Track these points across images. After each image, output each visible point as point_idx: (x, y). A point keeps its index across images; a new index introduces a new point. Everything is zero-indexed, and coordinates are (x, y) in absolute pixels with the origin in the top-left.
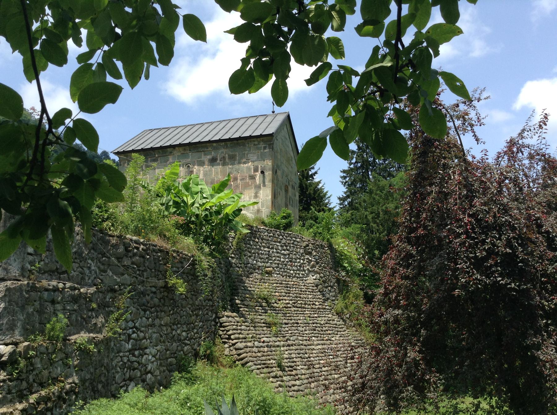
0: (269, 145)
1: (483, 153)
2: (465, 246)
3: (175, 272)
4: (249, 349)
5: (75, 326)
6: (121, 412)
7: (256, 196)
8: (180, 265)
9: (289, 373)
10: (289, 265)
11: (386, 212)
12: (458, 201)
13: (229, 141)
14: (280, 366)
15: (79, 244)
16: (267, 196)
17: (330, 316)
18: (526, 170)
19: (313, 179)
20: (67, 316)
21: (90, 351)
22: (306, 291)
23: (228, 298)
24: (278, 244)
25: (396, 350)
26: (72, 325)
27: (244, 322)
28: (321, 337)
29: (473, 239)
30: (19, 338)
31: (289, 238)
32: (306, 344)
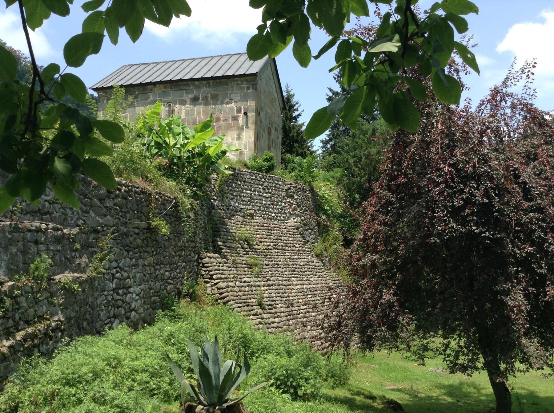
0: (253, 85)
1: (467, 102)
2: (443, 195)
4: (230, 289)
6: (107, 349)
7: (239, 138)
8: (162, 207)
9: (269, 311)
10: (271, 208)
11: (368, 156)
12: (440, 151)
13: (211, 80)
14: (260, 304)
16: (250, 138)
17: (310, 257)
18: (508, 120)
19: (297, 121)
21: (75, 290)
23: (211, 240)
24: (260, 187)
27: (226, 263)
29: (452, 188)
30: (4, 277)
31: (271, 181)
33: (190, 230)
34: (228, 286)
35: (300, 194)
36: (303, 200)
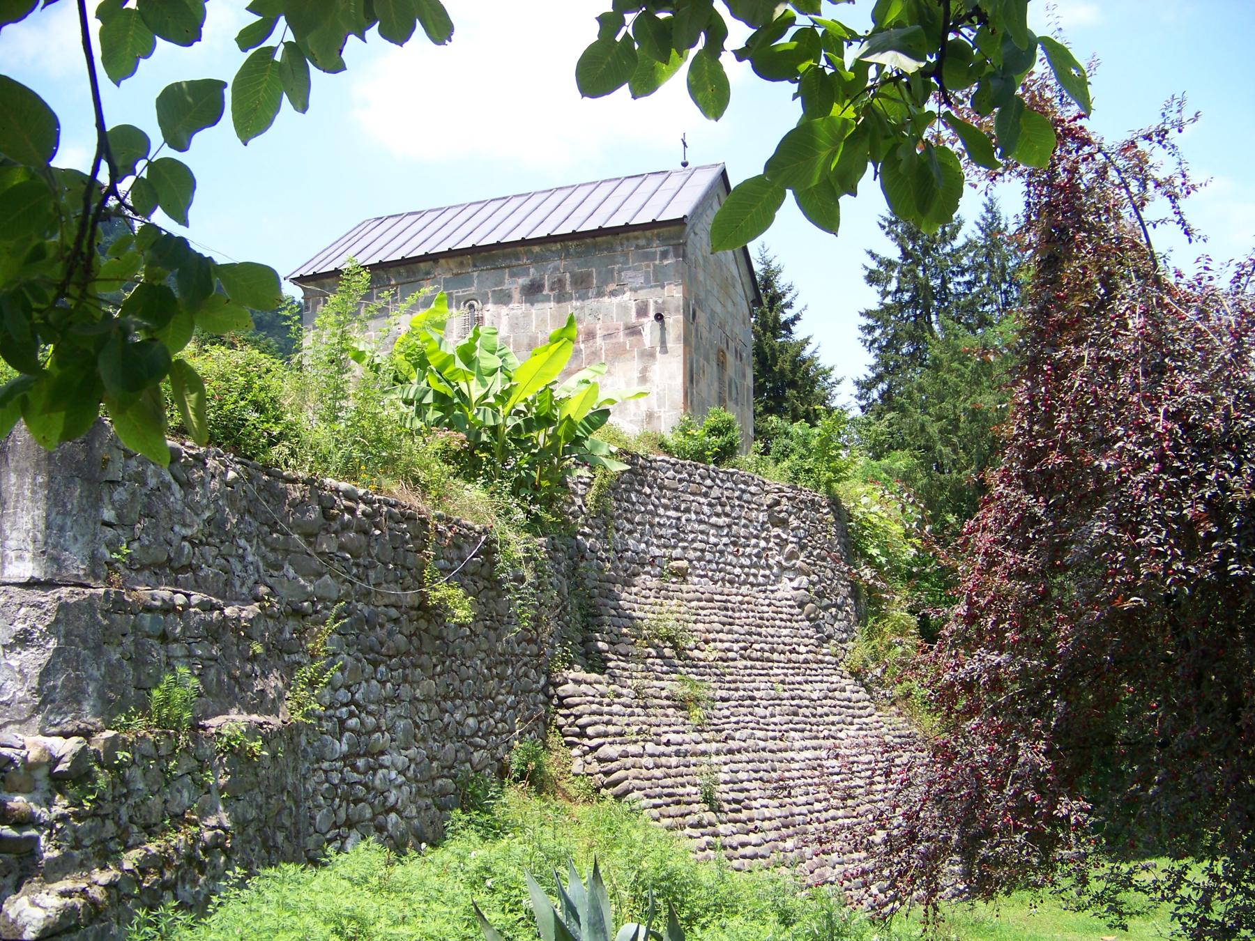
0: (676, 247)
3: (444, 571)
5: (217, 696)
7: (643, 379)
8: (454, 554)
9: (731, 815)
11: (974, 414)
12: (1142, 380)
13: (572, 239)
14: (708, 799)
15: (216, 501)
20: (196, 672)
21: (254, 755)
22: (774, 619)
24: (702, 500)
25: (992, 750)
26: (208, 692)
28: (811, 731)
29: (1177, 472)
31: (728, 485)
32: (775, 748)
33: (524, 612)
34: (625, 755)
35: (806, 516)
36: (813, 531)
